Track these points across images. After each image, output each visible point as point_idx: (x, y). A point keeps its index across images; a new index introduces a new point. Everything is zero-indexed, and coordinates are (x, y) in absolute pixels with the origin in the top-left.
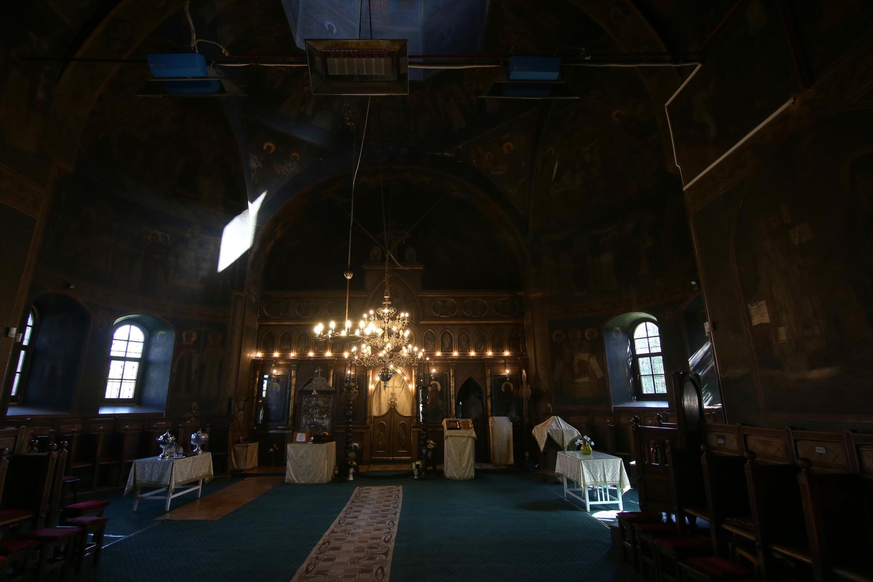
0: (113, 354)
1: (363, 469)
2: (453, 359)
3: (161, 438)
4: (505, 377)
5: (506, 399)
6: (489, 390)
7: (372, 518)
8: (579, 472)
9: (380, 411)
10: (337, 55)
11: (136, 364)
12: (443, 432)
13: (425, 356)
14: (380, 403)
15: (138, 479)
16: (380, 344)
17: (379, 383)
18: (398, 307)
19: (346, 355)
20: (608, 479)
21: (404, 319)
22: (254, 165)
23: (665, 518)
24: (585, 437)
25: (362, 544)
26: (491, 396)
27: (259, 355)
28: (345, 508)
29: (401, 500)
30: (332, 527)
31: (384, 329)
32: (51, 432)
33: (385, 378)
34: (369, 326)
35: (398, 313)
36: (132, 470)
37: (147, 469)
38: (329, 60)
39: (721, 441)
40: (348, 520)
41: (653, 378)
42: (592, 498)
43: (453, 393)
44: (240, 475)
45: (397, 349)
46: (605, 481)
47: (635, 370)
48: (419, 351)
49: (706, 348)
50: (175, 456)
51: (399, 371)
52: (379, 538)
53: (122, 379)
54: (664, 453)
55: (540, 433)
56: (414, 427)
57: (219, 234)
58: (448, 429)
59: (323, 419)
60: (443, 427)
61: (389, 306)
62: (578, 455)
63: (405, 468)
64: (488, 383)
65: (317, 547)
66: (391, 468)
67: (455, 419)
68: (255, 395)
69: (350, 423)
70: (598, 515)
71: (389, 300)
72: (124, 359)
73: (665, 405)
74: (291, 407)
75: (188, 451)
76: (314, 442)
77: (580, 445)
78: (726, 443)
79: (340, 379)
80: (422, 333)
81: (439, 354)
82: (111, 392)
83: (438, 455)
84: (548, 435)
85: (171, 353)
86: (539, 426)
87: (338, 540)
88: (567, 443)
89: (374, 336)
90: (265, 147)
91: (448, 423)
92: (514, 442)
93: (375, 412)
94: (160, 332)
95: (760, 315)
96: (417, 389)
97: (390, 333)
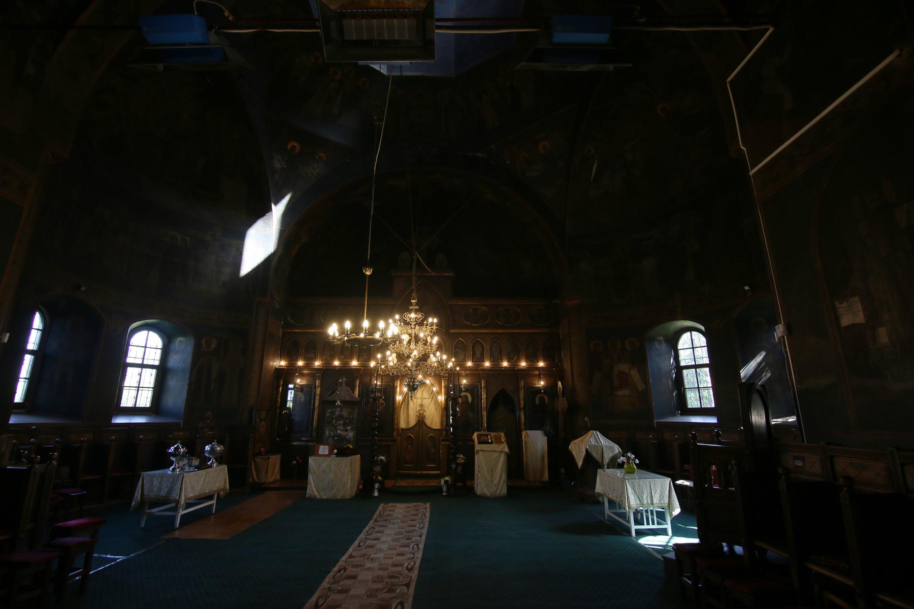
0: (129, 360)
1: (389, 484)
2: (485, 370)
3: (172, 449)
5: (540, 412)
6: (522, 403)
7: (394, 540)
8: (623, 493)
9: (408, 423)
10: (354, 16)
11: (154, 371)
12: (473, 446)
13: (455, 367)
14: (408, 415)
15: (146, 492)
16: (407, 349)
17: (407, 394)
18: (425, 309)
19: (372, 364)
20: (655, 501)
21: (432, 324)
22: (278, 165)
23: (726, 549)
24: (629, 454)
25: (381, 573)
27: (283, 363)
28: (367, 528)
29: (428, 519)
30: (351, 550)
31: (410, 335)
32: (33, 443)
33: (413, 388)
34: (391, 327)
35: (425, 319)
36: (140, 484)
37: (155, 482)
38: (345, 22)
39: (799, 463)
40: (369, 542)
41: (700, 390)
42: (637, 522)
43: (484, 405)
44: (259, 488)
45: (424, 358)
46: (652, 504)
47: (679, 382)
48: (448, 360)
49: (759, 359)
50: (187, 468)
51: (428, 382)
52: (401, 565)
53: (139, 387)
54: (723, 474)
55: (578, 449)
56: (443, 440)
57: (242, 237)
58: (479, 443)
60: (473, 441)
61: (416, 311)
62: (619, 473)
63: (433, 483)
64: (522, 394)
65: (331, 574)
66: (419, 483)
67: (486, 433)
68: (278, 405)
69: (376, 435)
70: (645, 541)
71: (417, 304)
72: (142, 366)
73: (713, 420)
74: (315, 417)
75: (203, 465)
76: (338, 455)
77: (623, 463)
78: (807, 465)
79: (367, 390)
80: (452, 340)
81: (469, 364)
82: (127, 400)
83: (469, 469)
84: (587, 450)
85: (189, 361)
87: (356, 566)
88: (606, 460)
89: (396, 339)
90: (289, 147)
91: (479, 436)
92: (549, 458)
93: (403, 425)
94: (179, 339)
95: (851, 314)
96: (447, 400)
97: (417, 339)
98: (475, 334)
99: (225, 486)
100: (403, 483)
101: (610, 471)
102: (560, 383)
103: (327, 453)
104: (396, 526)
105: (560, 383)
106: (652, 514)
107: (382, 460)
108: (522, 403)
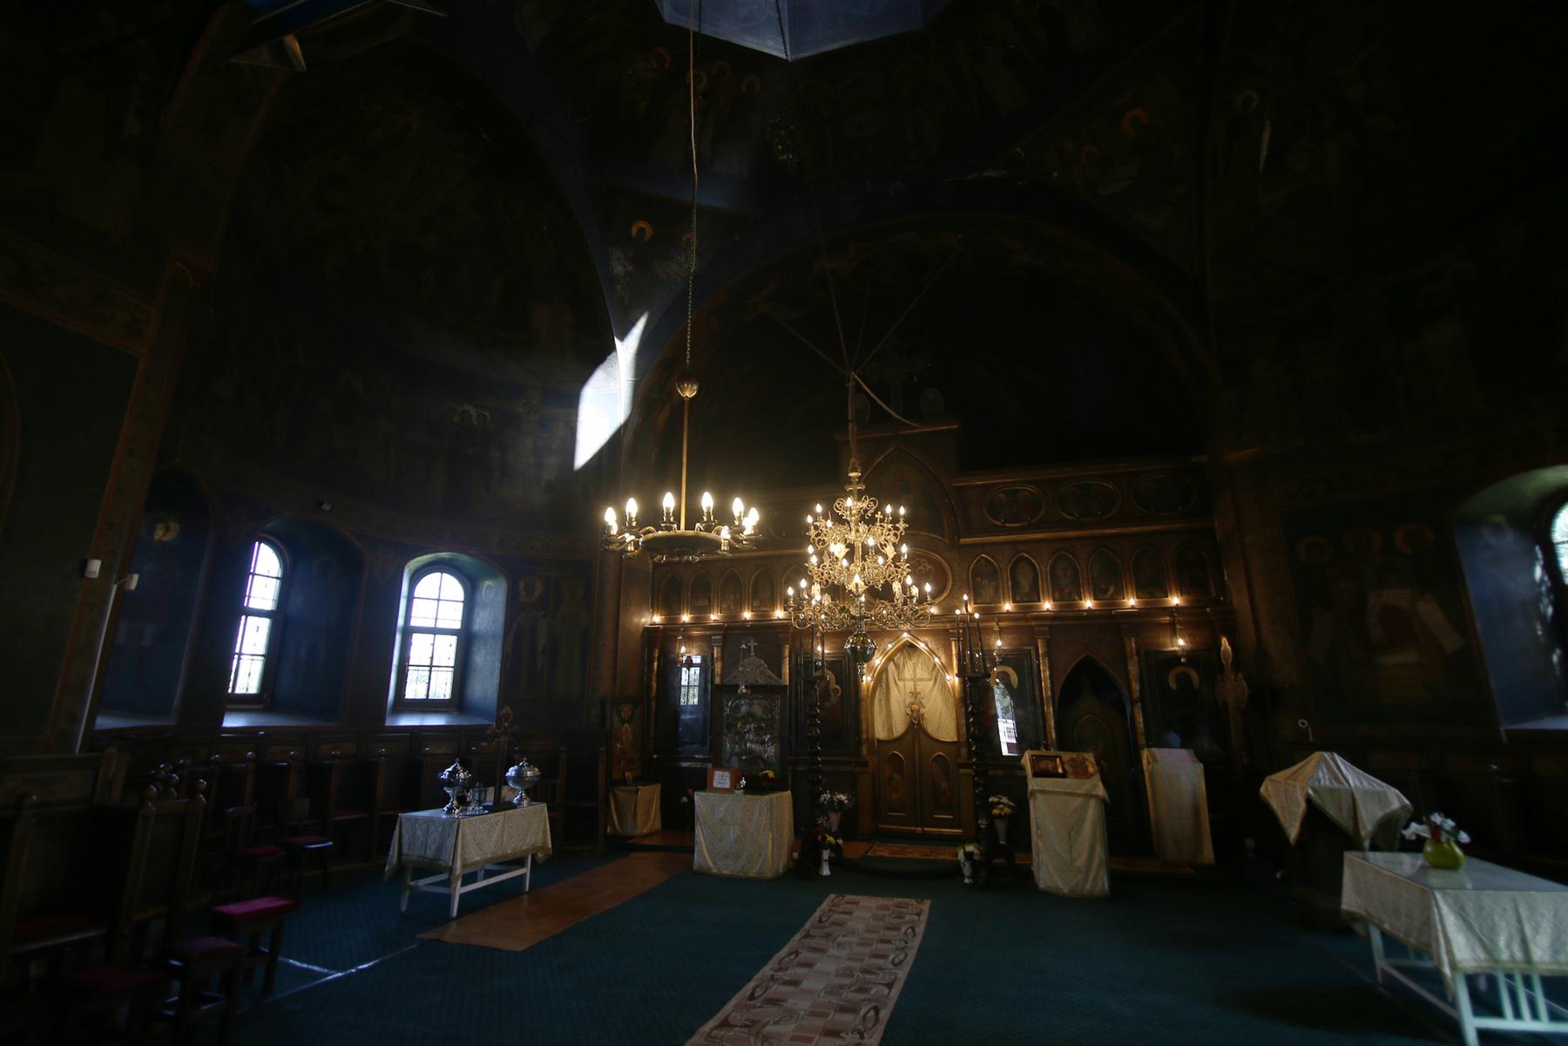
1: (855, 850)
3: (445, 775)
4: (1174, 657)
5: (1182, 706)
6: (1136, 686)
9: (890, 729)
11: (453, 640)
14: (889, 714)
15: (405, 851)
18: (877, 489)
22: (618, 269)
26: (1142, 699)
28: (783, 952)
32: (292, 757)
35: (880, 508)
43: (1047, 693)
44: (623, 846)
51: (922, 646)
53: (431, 666)
57: (573, 402)
59: (763, 743)
60: (1022, 769)
61: (859, 496)
62: (1407, 863)
63: (944, 855)
64: (1133, 669)
66: (916, 852)
67: (1053, 752)
68: (653, 693)
72: (435, 631)
76: (748, 790)
79: (805, 666)
81: (1008, 606)
82: (414, 690)
84: (1309, 801)
85: (501, 619)
86: (1280, 776)
90: (634, 231)
91: (1035, 760)
92: (1210, 811)
93: (880, 733)
94: (487, 583)
98: (1014, 543)
99: (545, 842)
100: (883, 851)
101: (1378, 858)
102: (1224, 641)
103: (727, 786)
104: (845, 953)
105: (1224, 641)
106: (1528, 982)
107: (841, 802)
108: (1136, 686)
